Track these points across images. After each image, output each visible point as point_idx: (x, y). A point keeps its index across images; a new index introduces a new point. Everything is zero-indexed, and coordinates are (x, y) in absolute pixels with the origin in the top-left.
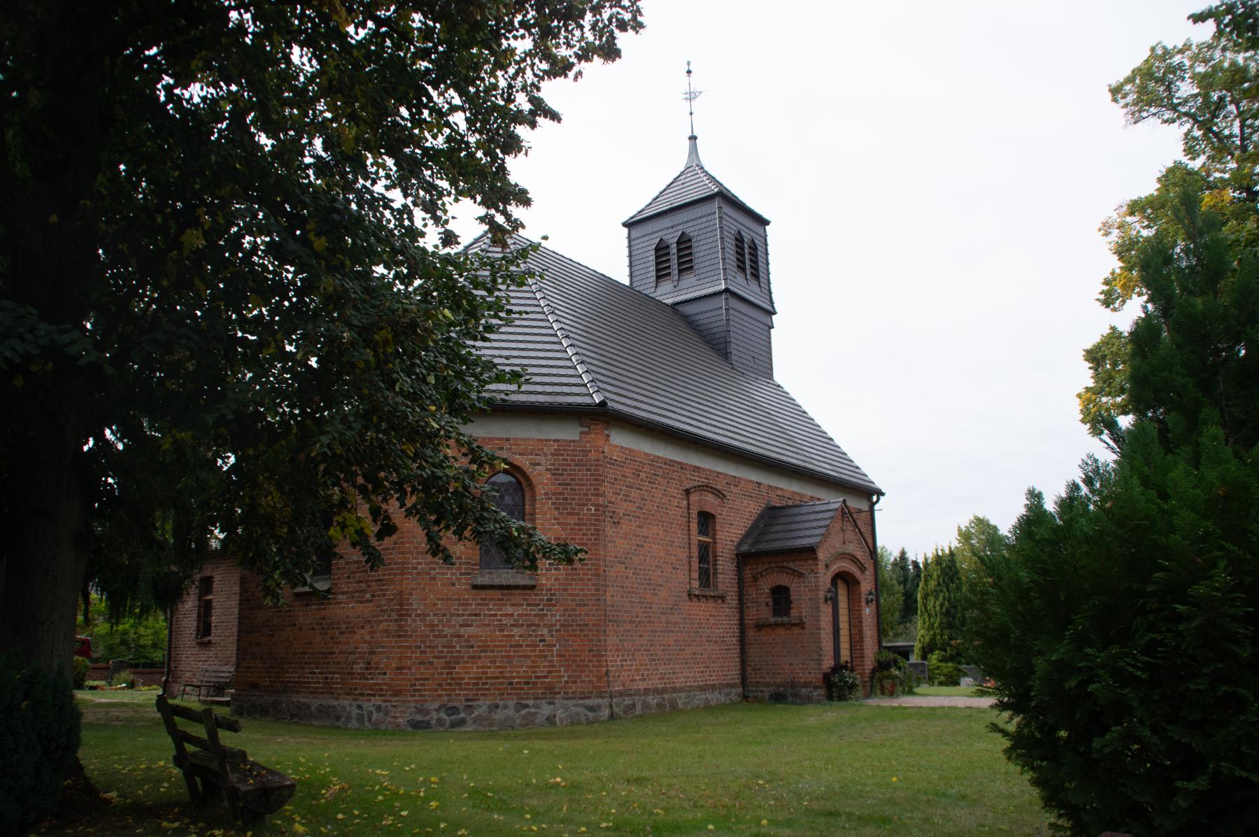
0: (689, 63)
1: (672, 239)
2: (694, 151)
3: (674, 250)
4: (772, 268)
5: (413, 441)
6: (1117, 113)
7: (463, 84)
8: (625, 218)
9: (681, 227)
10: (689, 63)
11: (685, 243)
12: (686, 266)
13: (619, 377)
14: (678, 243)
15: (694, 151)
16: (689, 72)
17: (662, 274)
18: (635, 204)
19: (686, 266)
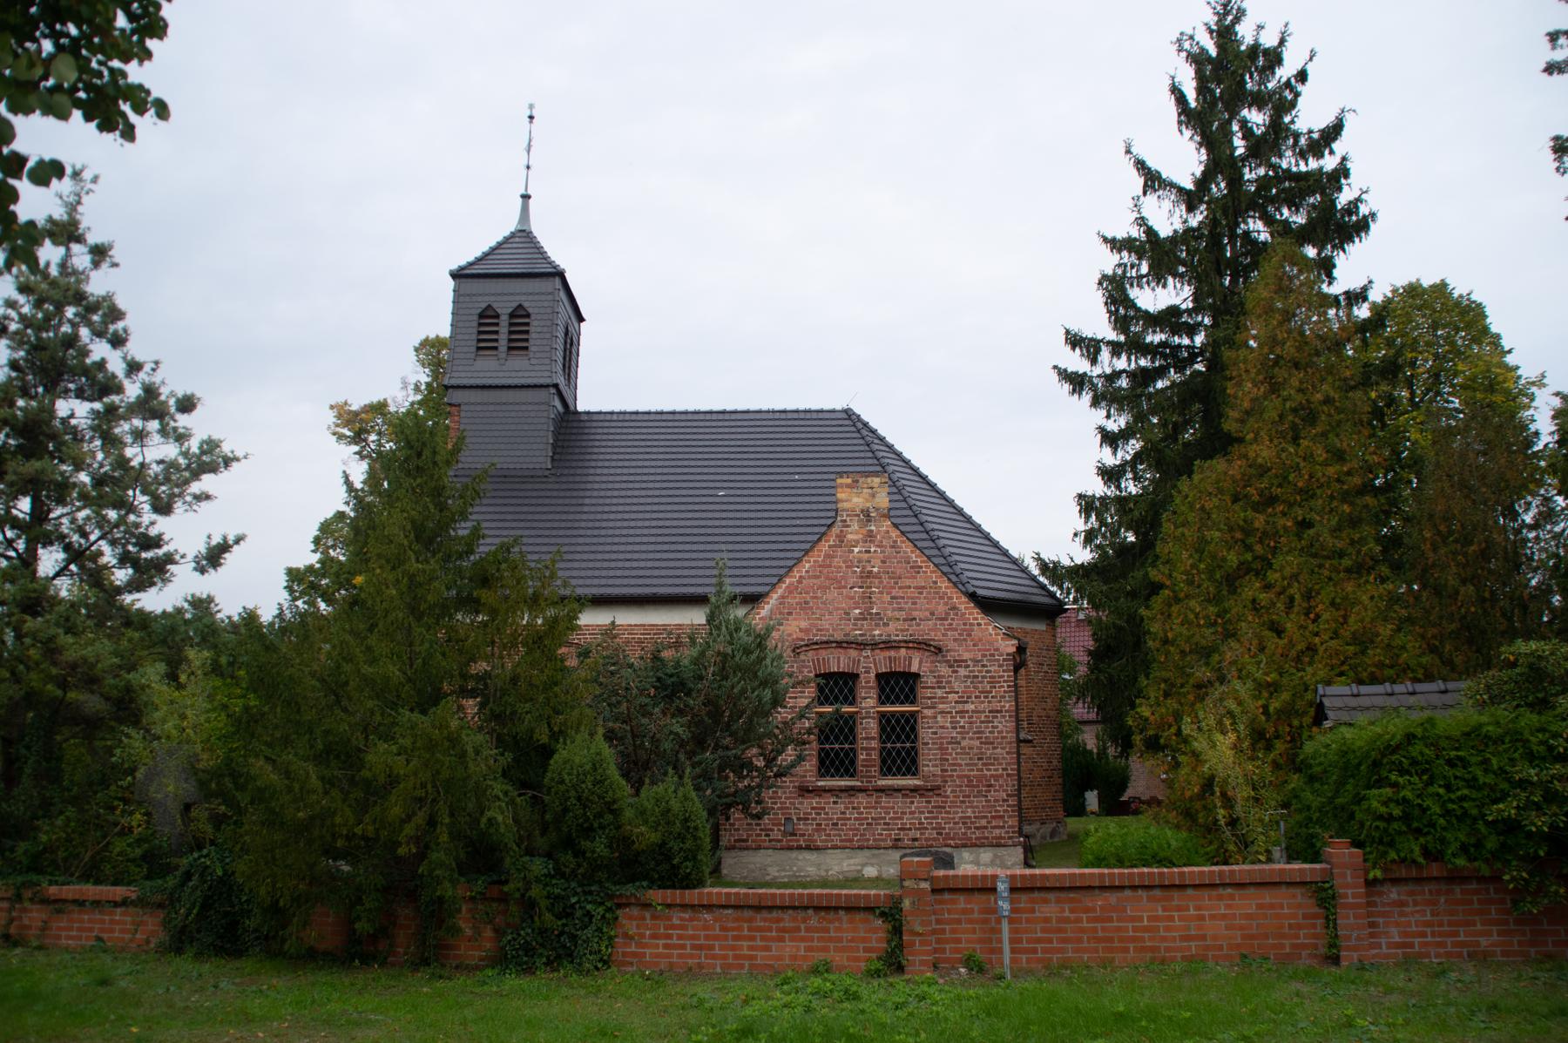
0: (531, 107)
1: (504, 309)
2: (525, 210)
3: (504, 321)
4: (680, 407)
5: (1525, 789)
6: (198, 394)
7: (133, 473)
8: (454, 267)
9: (523, 298)
10: (531, 107)
11: (520, 315)
12: (518, 344)
13: (709, 531)
14: (512, 315)
15: (525, 210)
16: (531, 117)
17: (485, 345)
18: (468, 251)
19: (518, 344)
